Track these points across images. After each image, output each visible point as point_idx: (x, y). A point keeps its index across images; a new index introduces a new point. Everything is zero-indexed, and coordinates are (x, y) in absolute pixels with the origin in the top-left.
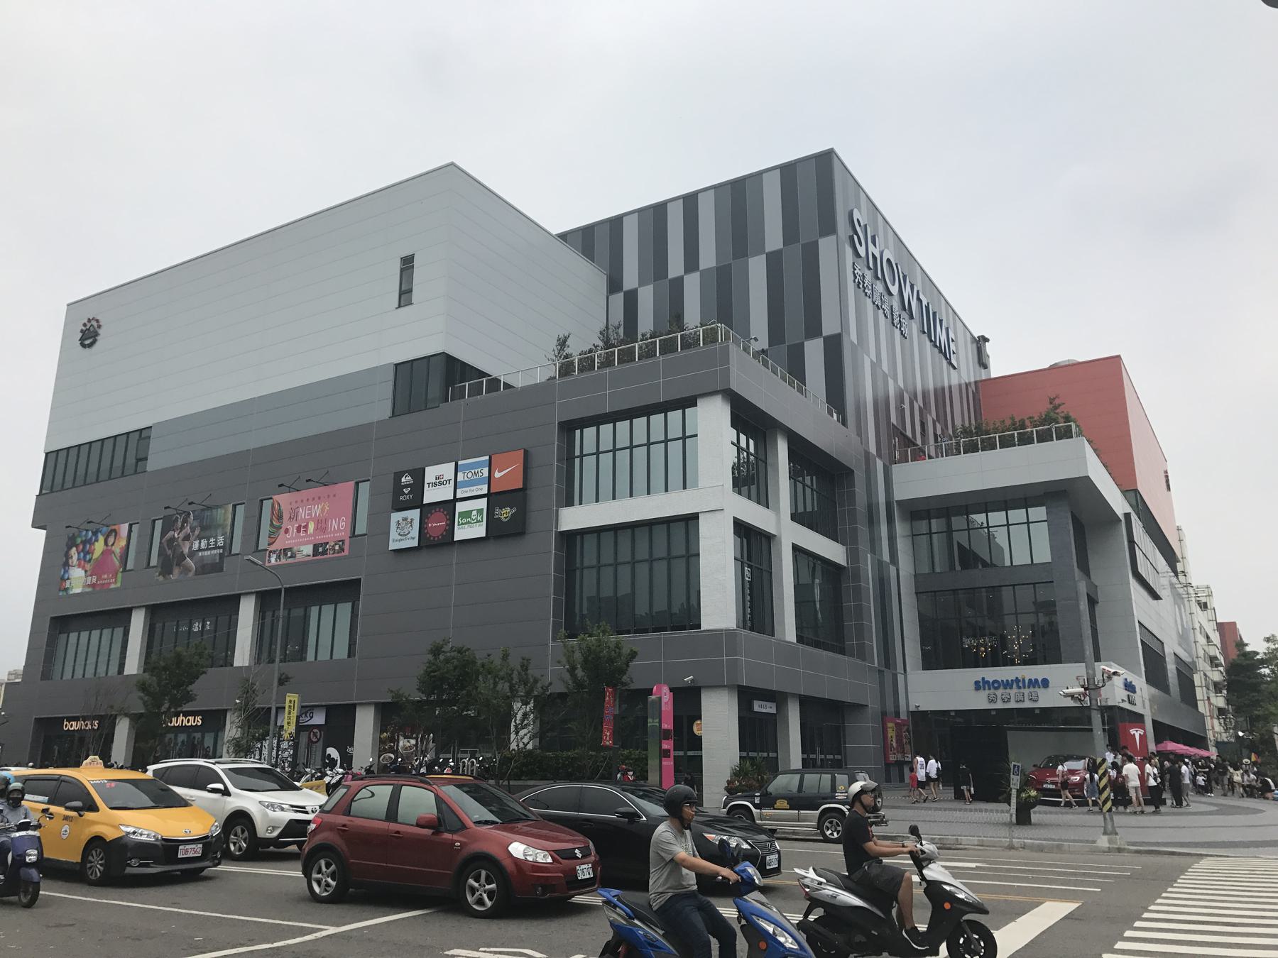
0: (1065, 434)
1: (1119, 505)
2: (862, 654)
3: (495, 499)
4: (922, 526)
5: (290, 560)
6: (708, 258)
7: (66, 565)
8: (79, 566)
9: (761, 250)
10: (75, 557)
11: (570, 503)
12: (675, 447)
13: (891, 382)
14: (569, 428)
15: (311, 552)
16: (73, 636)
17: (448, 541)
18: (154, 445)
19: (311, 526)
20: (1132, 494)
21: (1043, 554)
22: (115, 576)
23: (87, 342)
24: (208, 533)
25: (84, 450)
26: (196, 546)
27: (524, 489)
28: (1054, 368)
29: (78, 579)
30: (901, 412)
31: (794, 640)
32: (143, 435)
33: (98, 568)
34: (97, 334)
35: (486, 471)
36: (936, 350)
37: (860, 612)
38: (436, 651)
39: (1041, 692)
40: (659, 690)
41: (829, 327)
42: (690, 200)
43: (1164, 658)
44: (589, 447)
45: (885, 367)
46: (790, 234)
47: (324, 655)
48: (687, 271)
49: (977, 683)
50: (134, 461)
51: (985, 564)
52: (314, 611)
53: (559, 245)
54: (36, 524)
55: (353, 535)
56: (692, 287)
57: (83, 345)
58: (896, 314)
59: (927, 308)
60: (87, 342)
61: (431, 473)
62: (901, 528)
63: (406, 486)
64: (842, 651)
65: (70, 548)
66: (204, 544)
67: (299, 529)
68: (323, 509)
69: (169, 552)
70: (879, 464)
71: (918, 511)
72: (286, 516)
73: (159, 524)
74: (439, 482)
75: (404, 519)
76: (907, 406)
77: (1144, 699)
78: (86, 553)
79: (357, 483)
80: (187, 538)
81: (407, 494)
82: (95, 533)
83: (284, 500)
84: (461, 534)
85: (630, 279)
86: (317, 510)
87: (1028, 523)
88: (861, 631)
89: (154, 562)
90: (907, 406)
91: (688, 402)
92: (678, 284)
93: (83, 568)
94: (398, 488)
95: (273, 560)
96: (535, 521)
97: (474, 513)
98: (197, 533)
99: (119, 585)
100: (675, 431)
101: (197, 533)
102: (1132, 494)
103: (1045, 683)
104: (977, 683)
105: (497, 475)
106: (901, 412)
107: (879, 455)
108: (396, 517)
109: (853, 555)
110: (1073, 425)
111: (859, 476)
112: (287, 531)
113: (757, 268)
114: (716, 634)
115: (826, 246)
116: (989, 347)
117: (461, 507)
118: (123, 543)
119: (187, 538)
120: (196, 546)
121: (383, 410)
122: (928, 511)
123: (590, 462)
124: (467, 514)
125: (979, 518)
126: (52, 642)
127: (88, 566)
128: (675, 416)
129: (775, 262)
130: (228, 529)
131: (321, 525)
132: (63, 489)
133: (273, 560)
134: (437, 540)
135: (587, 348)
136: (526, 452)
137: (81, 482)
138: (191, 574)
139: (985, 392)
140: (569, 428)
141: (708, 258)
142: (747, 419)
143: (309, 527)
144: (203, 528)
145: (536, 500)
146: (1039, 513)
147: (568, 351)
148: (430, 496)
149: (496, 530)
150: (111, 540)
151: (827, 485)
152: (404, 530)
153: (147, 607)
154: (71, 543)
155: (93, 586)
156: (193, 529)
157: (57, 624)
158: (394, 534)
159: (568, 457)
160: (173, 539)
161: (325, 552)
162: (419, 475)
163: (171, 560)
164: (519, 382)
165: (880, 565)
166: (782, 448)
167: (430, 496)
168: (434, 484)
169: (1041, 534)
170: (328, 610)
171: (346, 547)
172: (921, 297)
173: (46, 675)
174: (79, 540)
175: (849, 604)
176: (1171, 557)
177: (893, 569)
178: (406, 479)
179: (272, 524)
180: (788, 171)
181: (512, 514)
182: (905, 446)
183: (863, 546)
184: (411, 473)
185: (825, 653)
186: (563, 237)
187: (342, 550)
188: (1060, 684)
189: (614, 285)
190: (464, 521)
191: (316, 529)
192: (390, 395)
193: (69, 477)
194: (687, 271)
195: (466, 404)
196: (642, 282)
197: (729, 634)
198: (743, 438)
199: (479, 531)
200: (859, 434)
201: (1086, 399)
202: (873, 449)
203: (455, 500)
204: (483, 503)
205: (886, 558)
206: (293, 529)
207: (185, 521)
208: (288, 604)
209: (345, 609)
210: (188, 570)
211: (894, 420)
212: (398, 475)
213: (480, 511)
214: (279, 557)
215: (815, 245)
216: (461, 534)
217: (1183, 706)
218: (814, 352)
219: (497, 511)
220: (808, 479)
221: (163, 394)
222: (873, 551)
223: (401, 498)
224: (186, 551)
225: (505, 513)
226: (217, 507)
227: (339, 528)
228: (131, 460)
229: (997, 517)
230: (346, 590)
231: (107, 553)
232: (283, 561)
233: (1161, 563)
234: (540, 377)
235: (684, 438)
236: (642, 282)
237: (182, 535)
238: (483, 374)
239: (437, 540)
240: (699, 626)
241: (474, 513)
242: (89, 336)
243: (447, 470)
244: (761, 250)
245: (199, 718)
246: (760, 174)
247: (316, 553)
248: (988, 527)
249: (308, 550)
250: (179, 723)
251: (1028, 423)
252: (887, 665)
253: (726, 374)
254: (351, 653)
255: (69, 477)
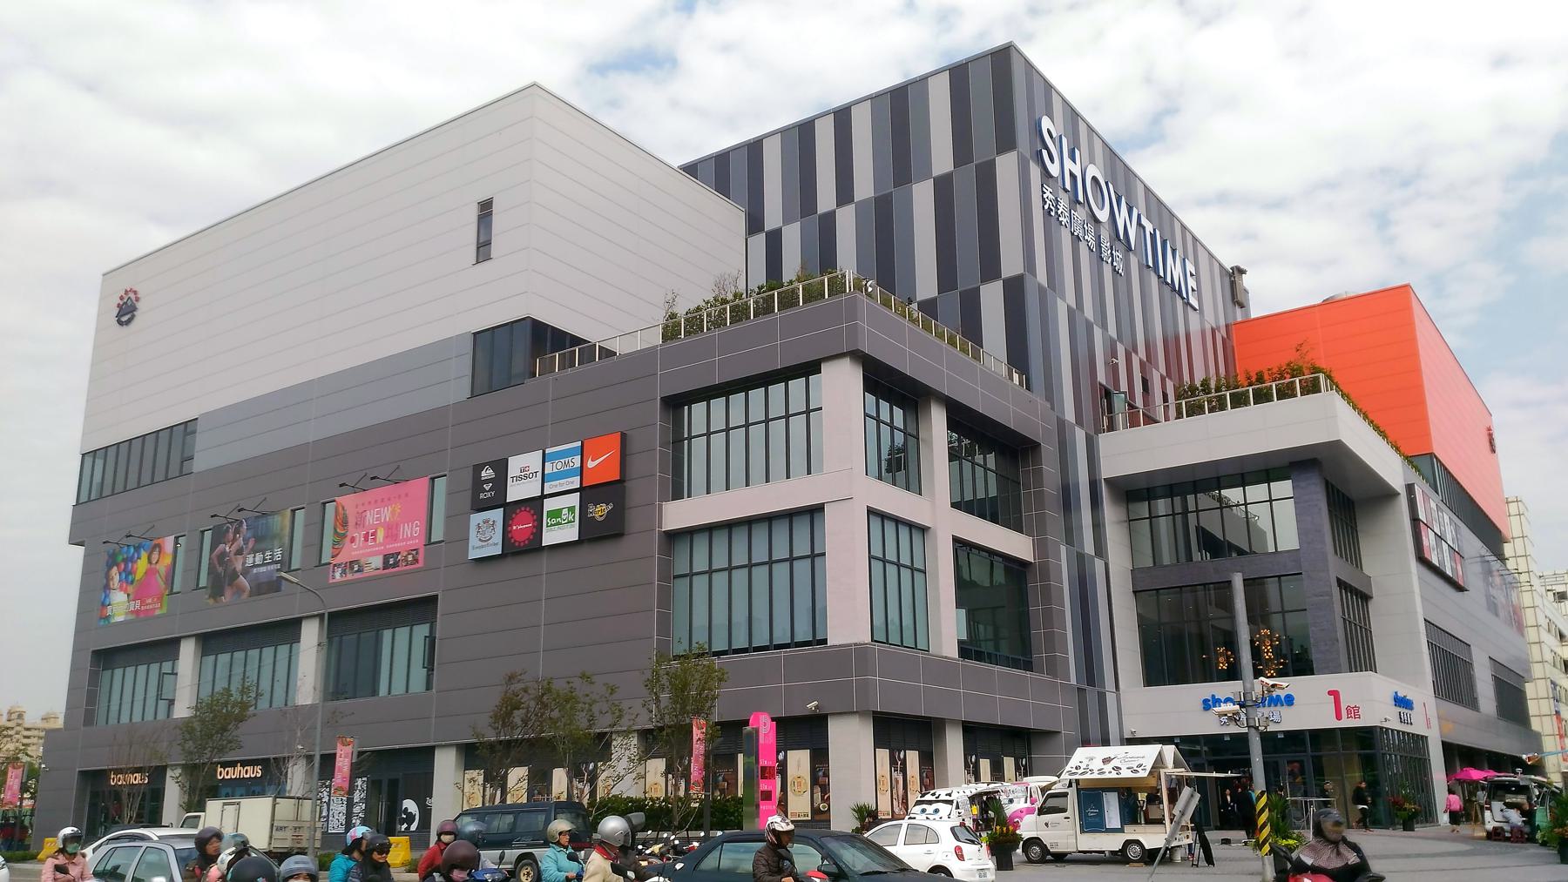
0: (1312, 388)
1: (1389, 467)
2: (1054, 668)
3: (589, 493)
4: (1143, 509)
5: (358, 575)
6: (864, 187)
7: (107, 587)
8: (121, 589)
9: (926, 174)
10: (117, 578)
11: (677, 495)
12: (798, 424)
13: (1097, 332)
14: (676, 404)
15: (380, 565)
16: (118, 672)
17: (533, 547)
18: (201, 441)
19: (381, 534)
20: (1423, 461)
21: (1288, 539)
22: (160, 599)
23: (124, 319)
24: (262, 546)
25: (124, 448)
26: (250, 561)
27: (621, 481)
28: (1328, 303)
29: (120, 604)
30: (1113, 370)
31: (952, 651)
32: (187, 428)
33: (141, 592)
34: (134, 309)
35: (577, 460)
36: (1167, 290)
37: (1049, 617)
38: (511, 678)
39: (1285, 711)
40: (757, 719)
41: (1011, 264)
42: (842, 117)
43: (1469, 665)
44: (699, 426)
45: (1089, 313)
46: (962, 151)
47: (399, 688)
48: (840, 204)
49: (1206, 701)
50: (179, 461)
51: (1241, 552)
52: (387, 634)
53: (688, 183)
54: (75, 540)
55: (429, 543)
56: (846, 223)
57: (120, 323)
58: (1106, 244)
59: (1153, 236)
60: (124, 319)
61: (515, 464)
62: (1111, 513)
63: (487, 482)
64: (1028, 666)
65: (110, 568)
66: (259, 557)
67: (366, 539)
68: (393, 513)
69: (220, 569)
70: (1080, 435)
71: (1135, 491)
72: (351, 521)
73: (208, 535)
74: (524, 476)
75: (486, 522)
76: (1121, 361)
77: (1430, 721)
78: (128, 573)
79: (433, 479)
80: (239, 552)
81: (487, 493)
82: (137, 549)
83: (349, 501)
84: (550, 537)
85: (773, 216)
86: (386, 514)
87: (1271, 501)
88: (1052, 641)
89: (203, 583)
90: (1121, 361)
91: (810, 369)
92: (829, 221)
93: (126, 591)
94: (478, 484)
95: (337, 575)
96: (635, 520)
97: (565, 511)
98: (251, 545)
99: (164, 611)
100: (797, 404)
101: (251, 545)
102: (1423, 461)
103: (1289, 700)
104: (1206, 701)
105: (591, 464)
106: (1113, 370)
107: (1079, 422)
108: (477, 518)
109: (1041, 547)
110: (1322, 376)
111: (1049, 451)
112: (353, 540)
113: (923, 196)
114: (844, 651)
115: (1006, 167)
116: (1246, 281)
117: (549, 505)
118: (168, 560)
119: (239, 552)
120: (250, 561)
121: (459, 390)
122: (1218, 478)
123: (699, 445)
124: (556, 514)
125: (1233, 494)
126: (94, 679)
127: (131, 589)
128: (797, 385)
129: (943, 187)
130: (286, 540)
131: (392, 531)
132: (101, 497)
133: (337, 575)
134: (522, 548)
135: (693, 307)
136: (623, 436)
137: (129, 485)
138: (245, 596)
139: (1240, 335)
140: (676, 404)
141: (864, 187)
142: (886, 383)
143: (379, 534)
144: (259, 539)
145: (636, 492)
146: (1283, 488)
147: (675, 310)
148: (515, 492)
149: (591, 533)
150: (155, 556)
151: (1001, 457)
152: (486, 535)
153: (198, 636)
154: (112, 562)
155: (137, 612)
156: (246, 541)
157: (103, 659)
158: (473, 540)
159: (678, 441)
160: (224, 554)
161: (396, 565)
162: (501, 467)
163: (222, 579)
164: (620, 347)
165: (1081, 561)
166: (938, 419)
167: (515, 492)
168: (519, 478)
169: (1286, 513)
170: (402, 633)
171: (421, 557)
172: (1144, 221)
173: (89, 719)
174: (120, 558)
175: (1036, 608)
176: (1491, 536)
177: (1099, 564)
178: (487, 473)
179: (336, 533)
180: (959, 74)
181: (609, 510)
182: (1103, 406)
183: (1055, 534)
184: (492, 465)
185: (997, 668)
186: (691, 169)
187: (416, 561)
188: (1308, 704)
189: (754, 224)
190: (554, 521)
191: (386, 537)
192: (469, 372)
193: (133, 477)
194: (840, 204)
195: (556, 376)
196: (787, 221)
197: (860, 649)
198: (884, 405)
199: (570, 533)
200: (1049, 397)
201: (1368, 341)
202: (1070, 416)
203: (543, 497)
204: (574, 500)
205: (1089, 548)
206: (359, 535)
207: (237, 531)
208: (356, 627)
209: (422, 631)
210: (240, 590)
211: (1101, 378)
212: (478, 468)
213: (571, 509)
214: (344, 572)
215: (991, 165)
216: (550, 537)
217: (1502, 723)
218: (992, 298)
219: (591, 508)
220: (979, 458)
221: (214, 376)
222: (1069, 541)
223: (482, 496)
224: (239, 567)
225: (600, 511)
226: (273, 513)
227: (412, 533)
228: (176, 458)
229: (1257, 492)
230: (421, 609)
231: (150, 573)
232: (350, 577)
233: (1473, 545)
234: (637, 344)
235: (808, 412)
236: (787, 221)
237: (234, 547)
238: (576, 341)
239: (522, 548)
240: (824, 641)
241: (565, 511)
242: (126, 312)
243: (533, 460)
244: (926, 174)
245: (258, 768)
246: (924, 79)
247: (386, 566)
248: (1246, 504)
249: (377, 561)
250: (236, 775)
251: (1266, 377)
252: (1091, 681)
253: (854, 330)
254: (429, 686)
255: (133, 477)
